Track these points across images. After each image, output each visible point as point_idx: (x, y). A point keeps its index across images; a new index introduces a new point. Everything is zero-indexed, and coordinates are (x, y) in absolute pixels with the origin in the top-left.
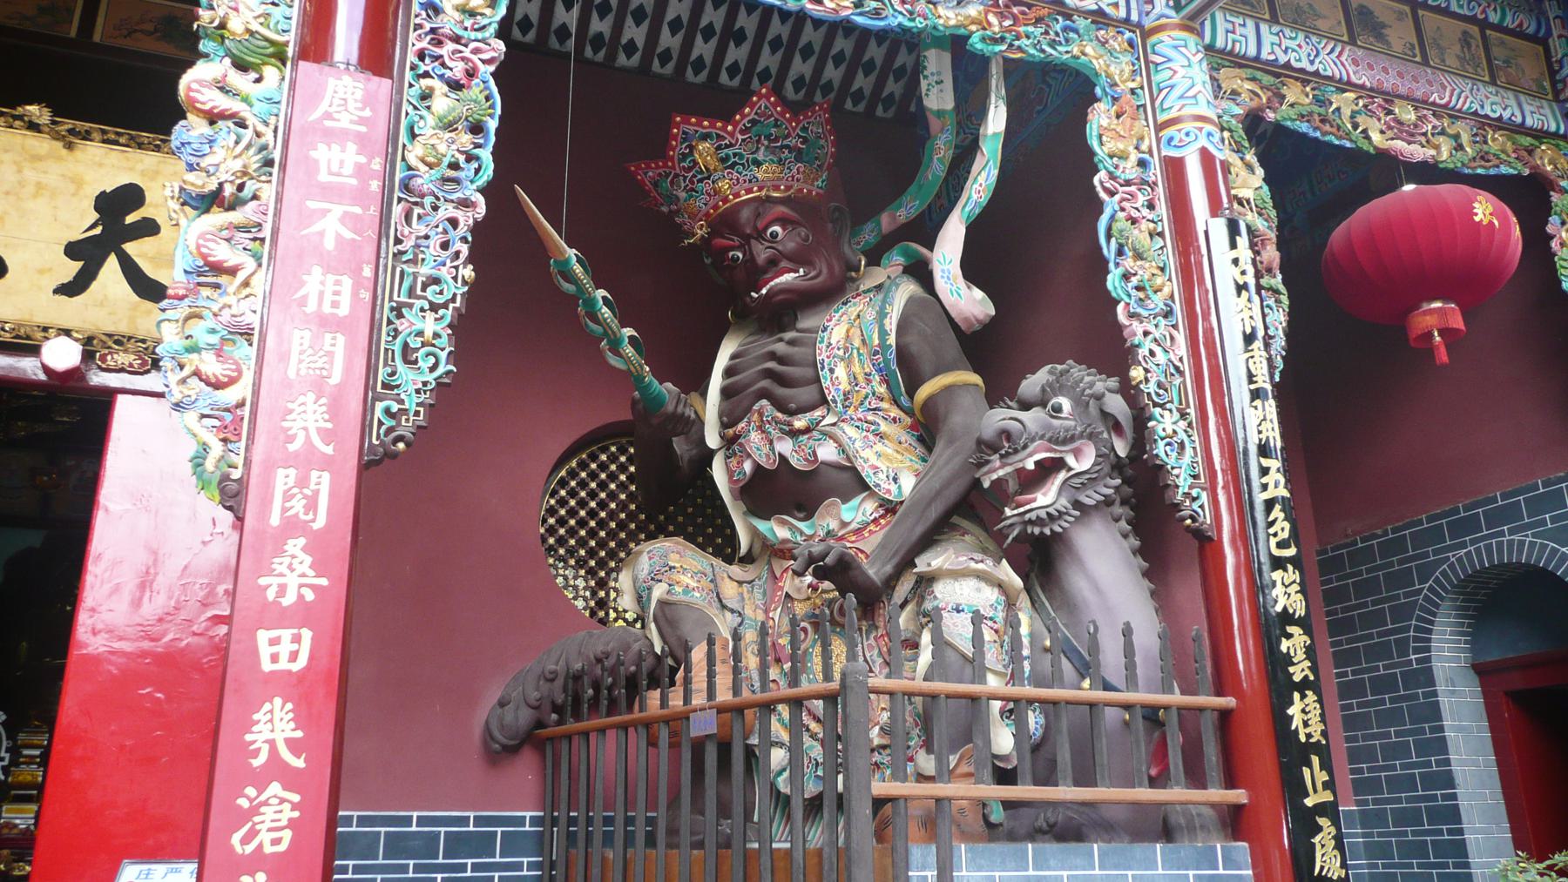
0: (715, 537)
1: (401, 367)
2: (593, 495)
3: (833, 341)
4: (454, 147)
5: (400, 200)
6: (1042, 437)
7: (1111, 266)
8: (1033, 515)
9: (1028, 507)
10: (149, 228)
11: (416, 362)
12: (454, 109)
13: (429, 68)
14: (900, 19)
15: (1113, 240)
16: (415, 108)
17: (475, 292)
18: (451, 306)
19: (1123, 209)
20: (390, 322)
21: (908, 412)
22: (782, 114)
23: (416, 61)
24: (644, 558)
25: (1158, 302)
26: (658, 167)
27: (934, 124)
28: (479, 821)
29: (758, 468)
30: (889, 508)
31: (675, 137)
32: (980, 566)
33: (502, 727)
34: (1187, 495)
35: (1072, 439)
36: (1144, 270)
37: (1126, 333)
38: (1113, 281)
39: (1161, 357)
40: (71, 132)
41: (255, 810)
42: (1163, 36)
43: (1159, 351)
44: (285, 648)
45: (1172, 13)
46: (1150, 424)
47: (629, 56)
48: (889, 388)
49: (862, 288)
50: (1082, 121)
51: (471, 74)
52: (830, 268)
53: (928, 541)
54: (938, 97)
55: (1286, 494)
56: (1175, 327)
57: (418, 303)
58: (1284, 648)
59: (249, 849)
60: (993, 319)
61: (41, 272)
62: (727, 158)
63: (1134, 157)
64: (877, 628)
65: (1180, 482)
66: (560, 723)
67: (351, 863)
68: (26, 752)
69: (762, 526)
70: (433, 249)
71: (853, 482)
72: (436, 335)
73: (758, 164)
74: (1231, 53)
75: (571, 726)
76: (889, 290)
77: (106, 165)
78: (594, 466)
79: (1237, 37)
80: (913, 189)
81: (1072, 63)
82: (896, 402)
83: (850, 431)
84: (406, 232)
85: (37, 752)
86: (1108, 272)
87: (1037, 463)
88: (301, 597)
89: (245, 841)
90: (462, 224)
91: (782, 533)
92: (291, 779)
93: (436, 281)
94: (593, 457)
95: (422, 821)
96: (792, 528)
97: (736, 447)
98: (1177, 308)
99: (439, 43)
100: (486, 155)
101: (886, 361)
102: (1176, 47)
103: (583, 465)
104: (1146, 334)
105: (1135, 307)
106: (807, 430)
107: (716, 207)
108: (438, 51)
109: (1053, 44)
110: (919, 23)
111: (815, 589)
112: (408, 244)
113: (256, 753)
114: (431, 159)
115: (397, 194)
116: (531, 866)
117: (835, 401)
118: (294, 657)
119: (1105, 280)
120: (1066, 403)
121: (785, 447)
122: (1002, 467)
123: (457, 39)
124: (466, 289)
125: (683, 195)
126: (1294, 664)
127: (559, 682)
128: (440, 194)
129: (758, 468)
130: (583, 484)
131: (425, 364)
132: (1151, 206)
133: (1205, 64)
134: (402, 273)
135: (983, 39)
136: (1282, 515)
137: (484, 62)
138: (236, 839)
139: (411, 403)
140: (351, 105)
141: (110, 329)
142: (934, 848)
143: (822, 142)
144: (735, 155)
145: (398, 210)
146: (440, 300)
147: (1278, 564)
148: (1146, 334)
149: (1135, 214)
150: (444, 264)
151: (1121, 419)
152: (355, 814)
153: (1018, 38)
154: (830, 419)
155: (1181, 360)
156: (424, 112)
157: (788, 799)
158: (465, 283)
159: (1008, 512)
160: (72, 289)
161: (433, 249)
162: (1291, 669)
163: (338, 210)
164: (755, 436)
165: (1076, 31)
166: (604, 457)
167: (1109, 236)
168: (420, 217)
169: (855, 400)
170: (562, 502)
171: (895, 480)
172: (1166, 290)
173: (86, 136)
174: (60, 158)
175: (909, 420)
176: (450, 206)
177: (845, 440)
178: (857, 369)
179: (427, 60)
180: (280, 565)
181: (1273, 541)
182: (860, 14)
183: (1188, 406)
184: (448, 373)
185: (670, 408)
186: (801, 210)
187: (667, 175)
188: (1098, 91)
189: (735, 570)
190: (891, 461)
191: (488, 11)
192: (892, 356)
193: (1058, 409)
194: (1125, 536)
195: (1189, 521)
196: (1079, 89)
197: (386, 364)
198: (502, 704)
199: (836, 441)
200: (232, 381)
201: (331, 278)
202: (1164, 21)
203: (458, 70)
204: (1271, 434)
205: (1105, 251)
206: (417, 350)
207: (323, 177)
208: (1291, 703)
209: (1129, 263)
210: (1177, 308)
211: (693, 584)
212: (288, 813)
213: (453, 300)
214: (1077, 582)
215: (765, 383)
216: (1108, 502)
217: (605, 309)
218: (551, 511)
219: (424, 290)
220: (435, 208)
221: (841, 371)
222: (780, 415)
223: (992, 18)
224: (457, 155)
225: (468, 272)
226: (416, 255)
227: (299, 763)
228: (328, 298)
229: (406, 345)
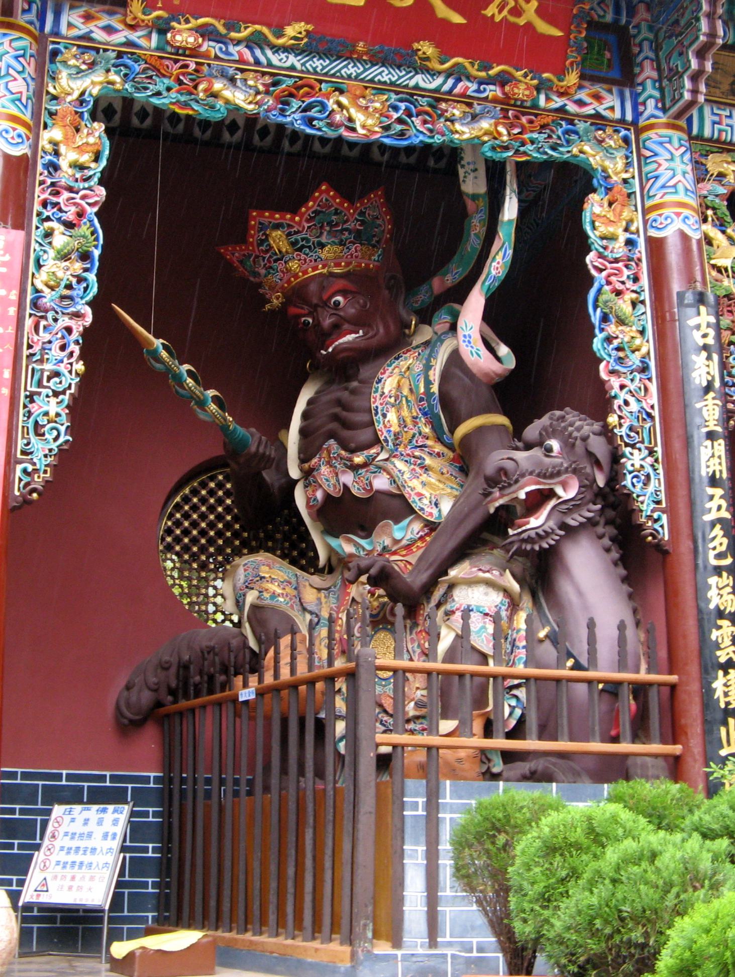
0: (300, 554)
2: (203, 517)
3: (386, 391)
4: (69, 273)
5: (31, 315)
6: (531, 473)
7: (597, 331)
8: (525, 535)
9: (524, 528)
11: (43, 435)
12: (68, 244)
13: (50, 214)
14: (421, 138)
15: (599, 310)
16: (41, 245)
17: (85, 380)
18: (68, 392)
19: (609, 283)
20: (25, 406)
21: (450, 447)
22: (341, 204)
23: (41, 209)
24: (241, 570)
25: (635, 360)
26: (241, 250)
27: (470, 205)
28: (113, 778)
29: (328, 497)
30: (431, 526)
31: (253, 227)
32: (487, 575)
33: (128, 705)
34: (649, 517)
35: (559, 474)
36: (624, 335)
37: (607, 386)
38: (597, 344)
39: (634, 406)
42: (651, 133)
43: (633, 399)
45: (660, 114)
46: (623, 460)
47: (232, 134)
48: (433, 428)
49: (415, 343)
50: (580, 210)
51: (81, 214)
52: (387, 328)
53: (459, 554)
54: (473, 184)
55: (728, 516)
56: (650, 379)
57: (44, 391)
58: (713, 637)
60: (513, 372)
62: (297, 242)
63: (623, 237)
64: (418, 625)
65: (644, 507)
66: (175, 702)
67: (18, 807)
69: (334, 542)
70: (55, 352)
71: (399, 506)
73: (322, 246)
74: (718, 141)
75: (183, 704)
76: (435, 346)
78: (204, 492)
79: (723, 127)
80: (456, 258)
81: (573, 161)
82: (439, 439)
83: (400, 464)
84: (35, 340)
86: (594, 336)
87: (527, 494)
90: (75, 331)
91: (349, 549)
93: (57, 374)
94: (204, 485)
95: (70, 777)
96: (357, 545)
97: (311, 479)
98: (652, 364)
99: (57, 194)
100: (92, 277)
101: (431, 407)
102: (661, 143)
103: (195, 492)
104: (622, 387)
105: (613, 365)
106: (365, 465)
107: (289, 282)
108: (54, 199)
109: (554, 148)
110: (438, 139)
111: (373, 594)
112: (37, 349)
114: (52, 283)
115: (28, 311)
116: (155, 814)
117: (386, 441)
119: (592, 343)
120: (555, 444)
121: (348, 478)
122: (502, 496)
123: (70, 189)
124: (78, 379)
125: (263, 272)
126: (720, 649)
127: (173, 670)
128: (59, 310)
129: (328, 497)
130: (195, 508)
131: (50, 437)
132: (636, 279)
133: (687, 156)
134: (33, 369)
135: (493, 148)
136: (722, 533)
137: (89, 204)
142: (424, 781)
143: (379, 222)
144: (303, 239)
145: (29, 323)
146: (60, 388)
147: (718, 571)
148: (622, 387)
149: (620, 287)
150: (62, 361)
151: (599, 456)
152: (19, 770)
153: (523, 144)
154: (383, 456)
155: (652, 407)
156: (47, 248)
157: (343, 756)
158: (77, 374)
159: (511, 532)
161: (55, 352)
162: (718, 653)
164: (325, 470)
165: (576, 133)
166: (212, 485)
167: (595, 307)
168: (45, 327)
169: (405, 438)
170: (178, 524)
171: (436, 505)
172: (644, 350)
175: (451, 455)
176: (66, 318)
177: (395, 473)
178: (405, 413)
179: (49, 207)
181: (712, 554)
182: (388, 137)
183: (656, 445)
184: (67, 442)
185: (253, 449)
186: (358, 282)
187: (250, 256)
188: (595, 182)
189: (316, 580)
190: (433, 489)
191: (93, 165)
192: (436, 402)
193: (549, 450)
194: (608, 550)
195: (650, 538)
196: (574, 181)
197: (23, 437)
198: (128, 688)
199: (389, 473)
202: (653, 121)
203: (70, 214)
204: (717, 468)
205: (593, 319)
206: (44, 426)
208: (716, 678)
209: (612, 329)
210: (652, 364)
211: (279, 591)
213: (69, 387)
214: (565, 588)
215: (334, 426)
216: (591, 523)
217: (189, 380)
218: (169, 531)
219: (48, 381)
220: (56, 320)
221: (392, 416)
222: (343, 452)
223: (501, 129)
224: (71, 278)
225: (80, 367)
226: (42, 356)
229: (36, 423)
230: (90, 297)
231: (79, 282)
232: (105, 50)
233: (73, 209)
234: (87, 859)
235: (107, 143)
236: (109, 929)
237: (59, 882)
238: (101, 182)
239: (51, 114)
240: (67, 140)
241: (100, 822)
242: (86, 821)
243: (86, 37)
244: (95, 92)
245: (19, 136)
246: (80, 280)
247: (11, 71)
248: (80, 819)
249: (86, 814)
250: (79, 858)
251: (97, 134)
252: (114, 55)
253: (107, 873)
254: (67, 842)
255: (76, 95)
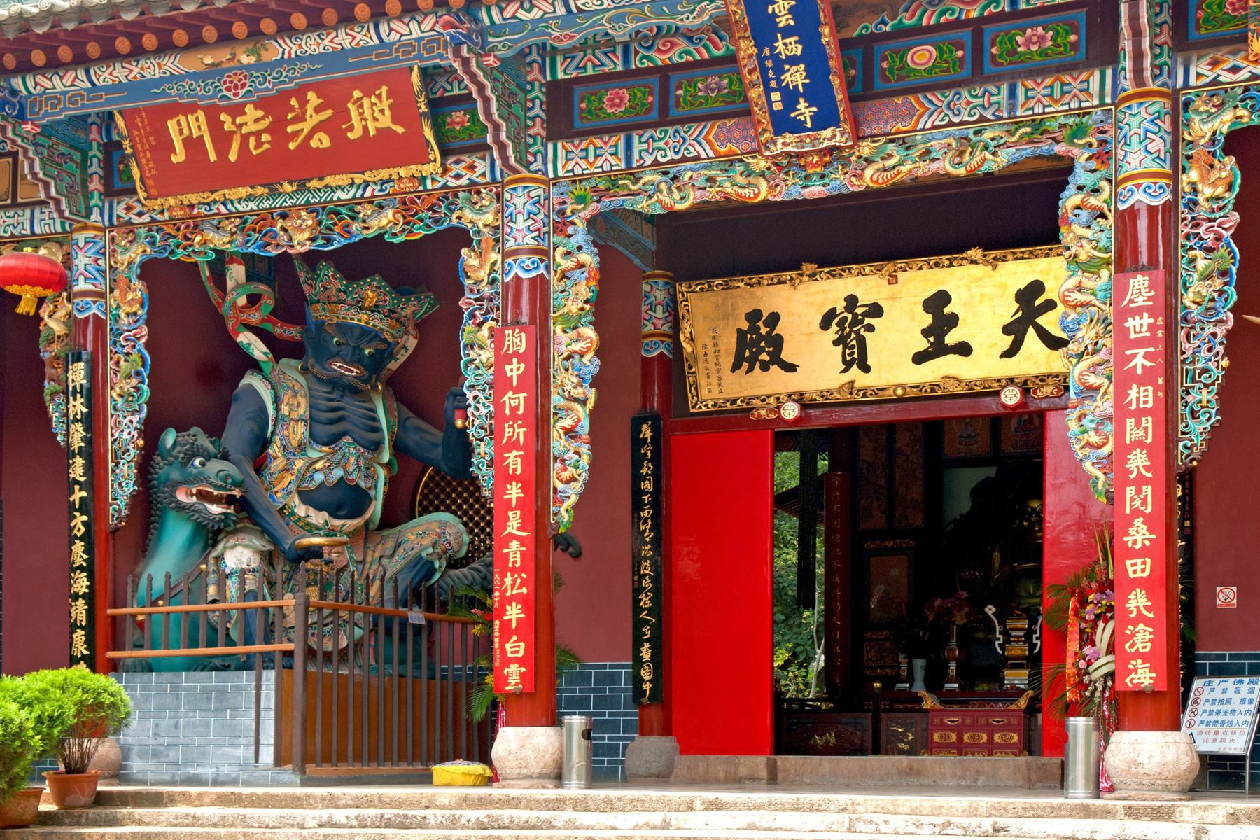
1: (1190, 422)
10: (1050, 305)
20: (113, 471)
40: (995, 259)
41: (1133, 635)
44: (1139, 567)
51: (1218, 239)
57: (1197, 385)
59: (1133, 650)
61: (991, 347)
68: (1014, 633)
70: (1204, 354)
72: (1208, 402)
77: (1018, 271)
85: (1022, 633)
88: (1144, 545)
89: (1131, 647)
92: (1147, 622)
99: (1197, 225)
112: (1189, 354)
113: (1131, 612)
118: (1143, 571)
137: (1225, 229)
138: (1127, 646)
139: (1198, 440)
140: (1143, 291)
141: (1035, 372)
160: (1010, 353)
161: (1204, 354)
163: (1142, 352)
173: (1004, 259)
174: (991, 276)
180: (1132, 531)
191: (1227, 195)
200: (1105, 444)
201: (1142, 389)
207: (1133, 336)
212: (1148, 636)
220: (1202, 329)
225: (1225, 363)
227: (1151, 615)
228: (1142, 399)
230: (1231, 304)
231: (1220, 295)
232: (1232, 89)
233: (1212, 236)
234: (1228, 718)
235: (1239, 173)
236: (1251, 774)
237: (1204, 736)
238: (1235, 209)
239: (1189, 157)
240: (1204, 178)
241: (1237, 691)
242: (1225, 691)
243: (1215, 82)
244: (1225, 130)
245: (1161, 187)
246: (1221, 293)
247: (1149, 135)
248: (1219, 689)
249: (1224, 685)
250: (1220, 718)
251: (1228, 168)
252: (1240, 91)
253: (1246, 729)
254: (1208, 707)
255: (1208, 135)
